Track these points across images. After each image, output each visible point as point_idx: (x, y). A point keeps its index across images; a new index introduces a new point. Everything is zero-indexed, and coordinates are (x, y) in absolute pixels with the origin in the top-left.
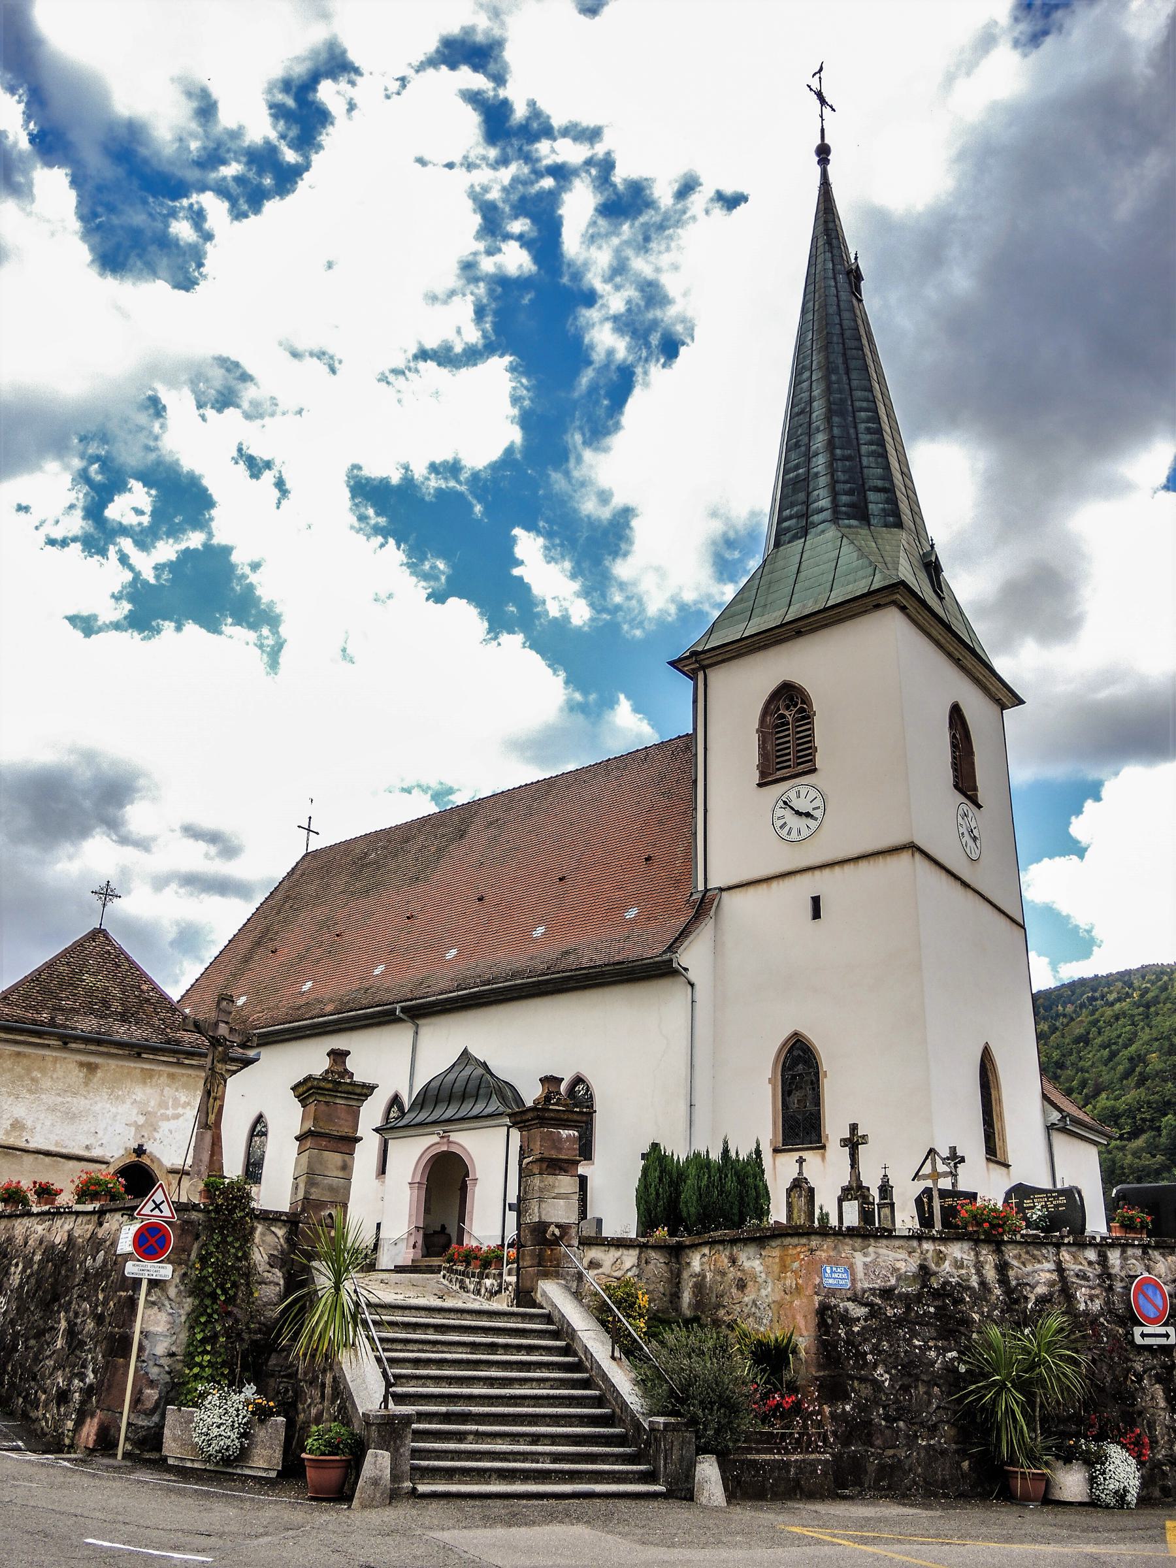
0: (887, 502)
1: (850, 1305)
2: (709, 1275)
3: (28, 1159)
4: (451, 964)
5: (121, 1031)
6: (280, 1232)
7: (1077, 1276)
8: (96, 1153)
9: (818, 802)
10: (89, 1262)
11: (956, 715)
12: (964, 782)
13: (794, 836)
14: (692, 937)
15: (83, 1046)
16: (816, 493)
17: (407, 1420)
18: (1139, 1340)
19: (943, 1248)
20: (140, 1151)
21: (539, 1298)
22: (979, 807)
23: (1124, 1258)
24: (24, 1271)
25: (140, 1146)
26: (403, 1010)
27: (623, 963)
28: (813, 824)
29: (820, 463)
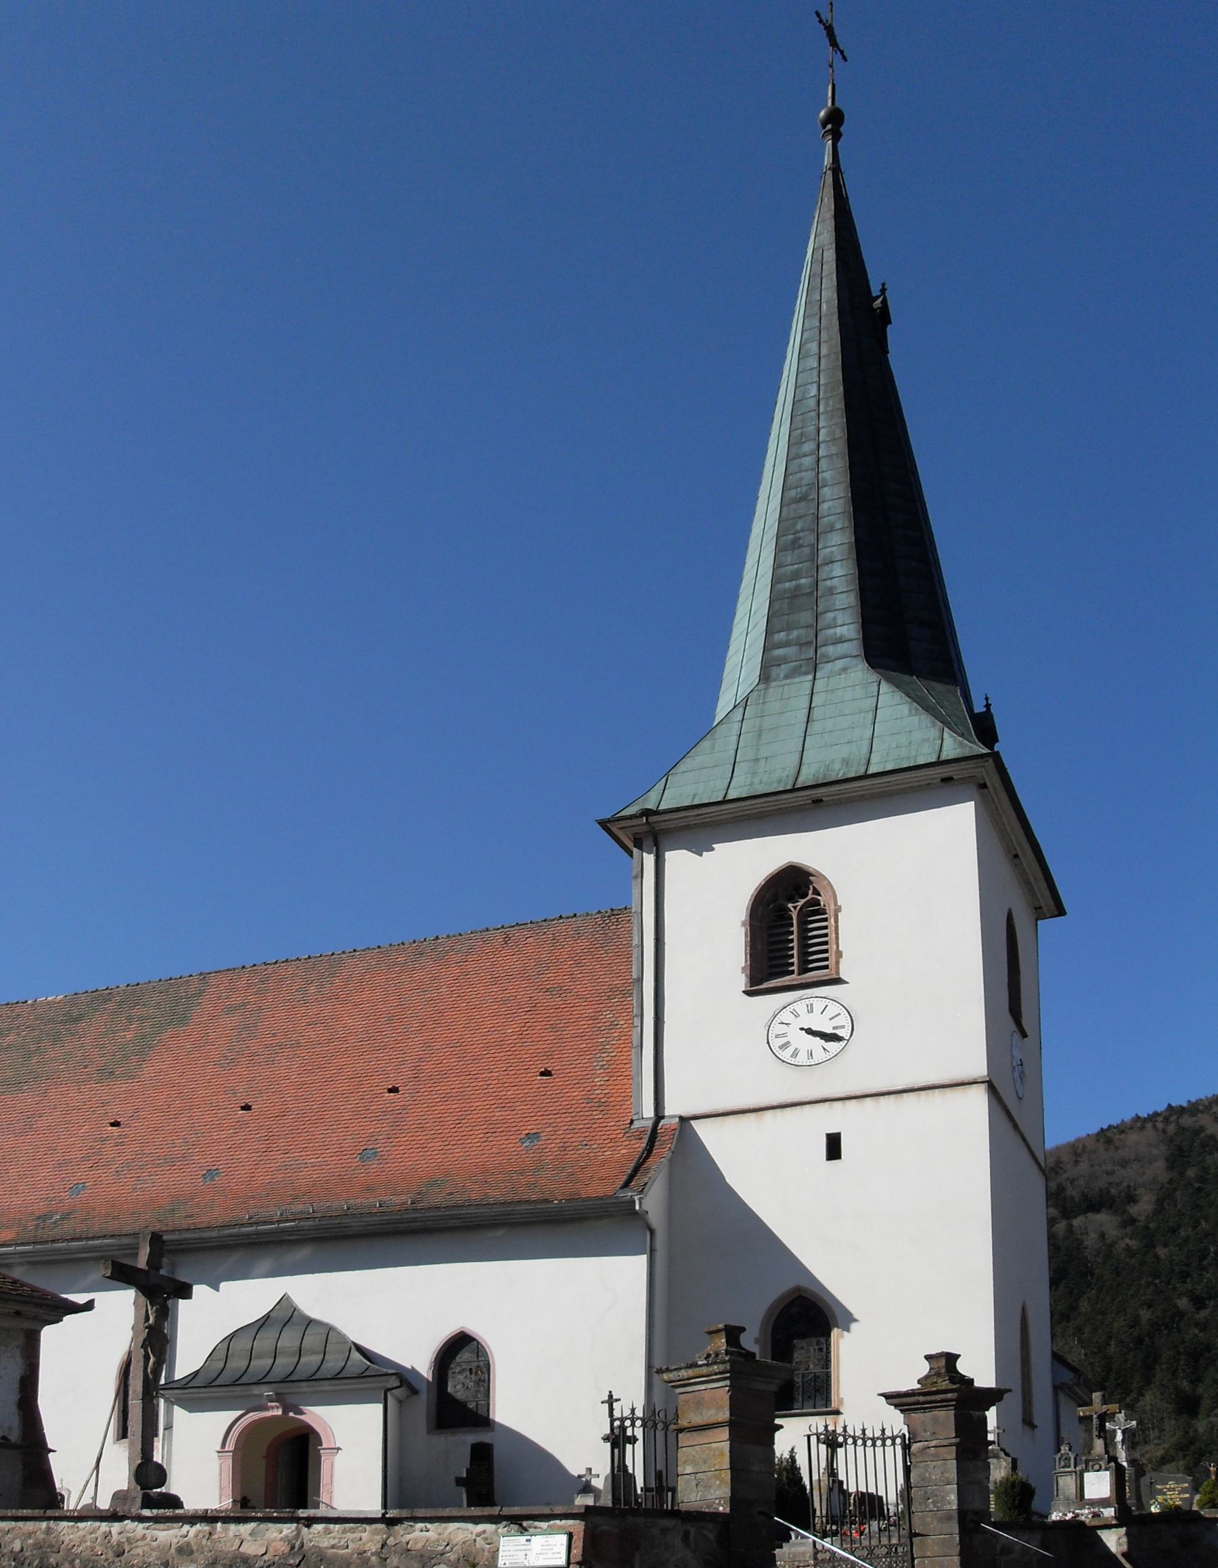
9: (844, 1020)
16: (830, 615)
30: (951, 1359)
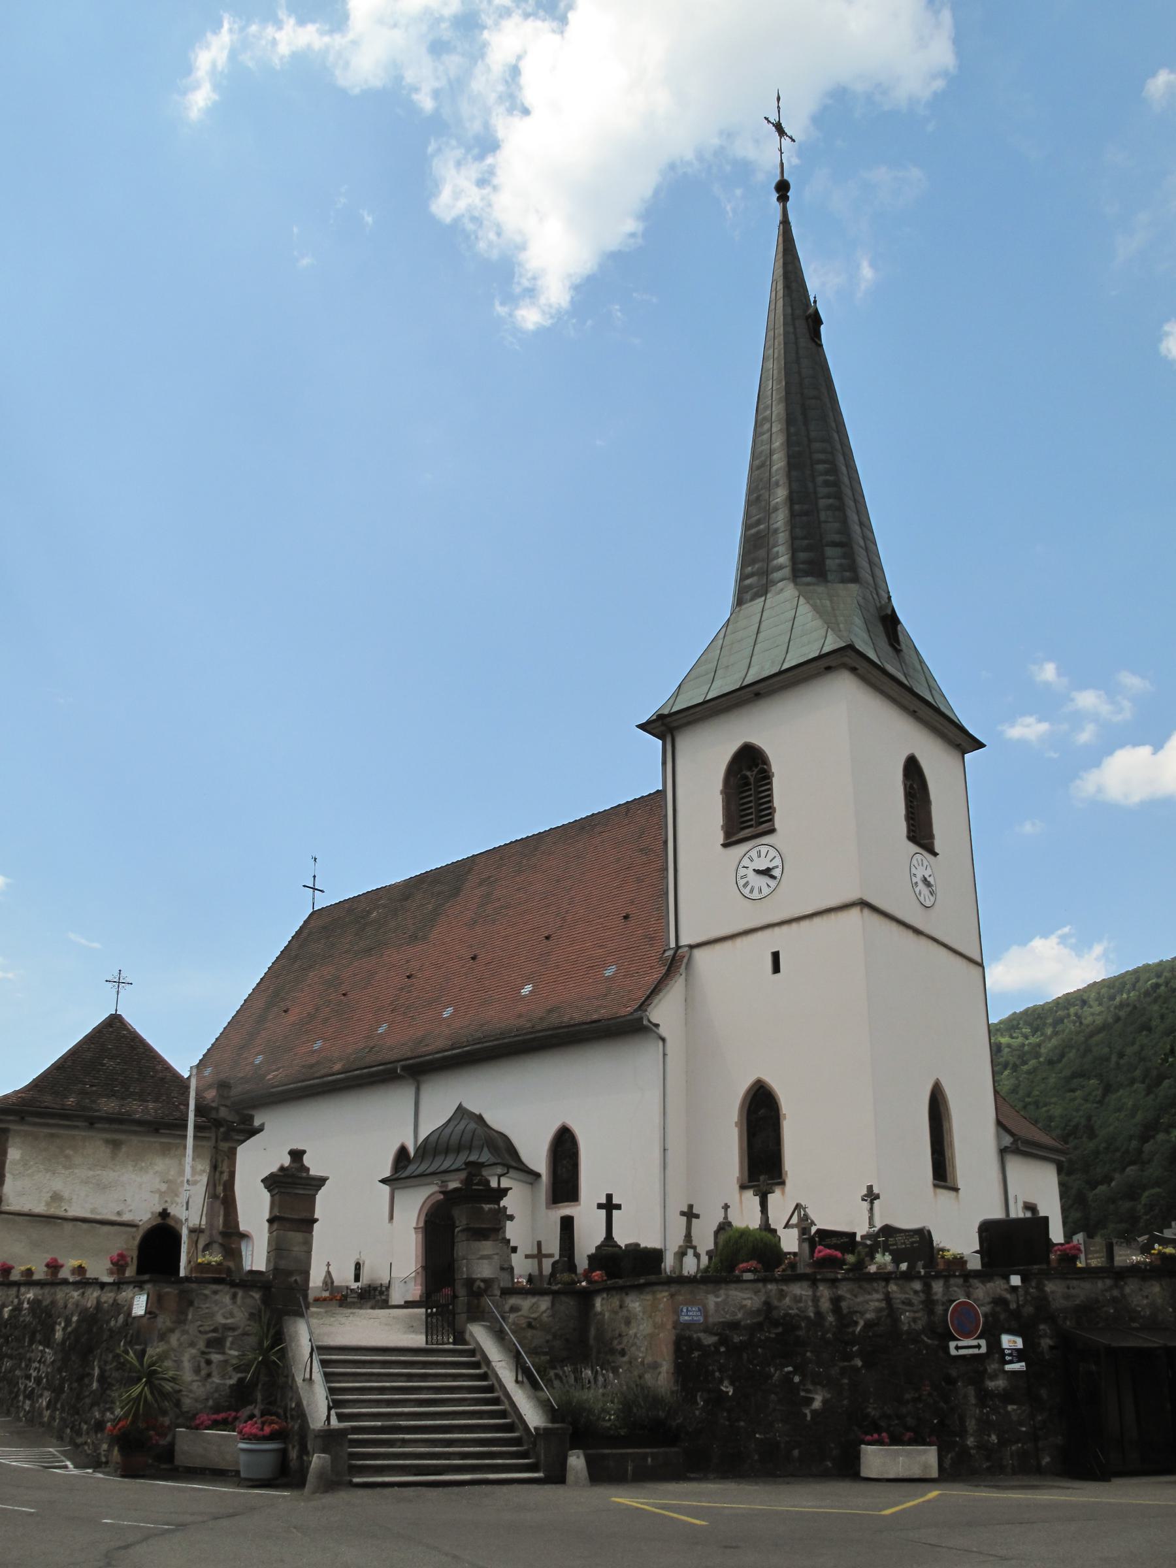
0: (844, 556)
1: (702, 1335)
2: (607, 1315)
3: (68, 1226)
4: (449, 1021)
5: (137, 1109)
6: (257, 1296)
7: (903, 1303)
8: (126, 1218)
9: (777, 862)
10: (112, 1323)
11: (913, 770)
12: (920, 830)
13: (756, 895)
14: (664, 992)
15: (107, 1126)
16: (776, 549)
17: (343, 1433)
18: (953, 1352)
19: (785, 1288)
20: (164, 1214)
21: (467, 1337)
22: (935, 854)
23: (947, 1286)
24: (64, 1329)
25: (165, 1210)
26: (404, 1068)
27: (599, 1021)
28: (773, 883)
29: (780, 519)
30: (301, 1153)
